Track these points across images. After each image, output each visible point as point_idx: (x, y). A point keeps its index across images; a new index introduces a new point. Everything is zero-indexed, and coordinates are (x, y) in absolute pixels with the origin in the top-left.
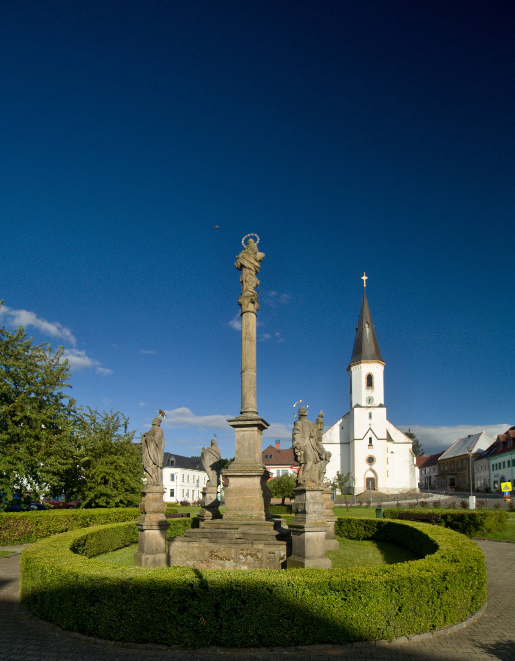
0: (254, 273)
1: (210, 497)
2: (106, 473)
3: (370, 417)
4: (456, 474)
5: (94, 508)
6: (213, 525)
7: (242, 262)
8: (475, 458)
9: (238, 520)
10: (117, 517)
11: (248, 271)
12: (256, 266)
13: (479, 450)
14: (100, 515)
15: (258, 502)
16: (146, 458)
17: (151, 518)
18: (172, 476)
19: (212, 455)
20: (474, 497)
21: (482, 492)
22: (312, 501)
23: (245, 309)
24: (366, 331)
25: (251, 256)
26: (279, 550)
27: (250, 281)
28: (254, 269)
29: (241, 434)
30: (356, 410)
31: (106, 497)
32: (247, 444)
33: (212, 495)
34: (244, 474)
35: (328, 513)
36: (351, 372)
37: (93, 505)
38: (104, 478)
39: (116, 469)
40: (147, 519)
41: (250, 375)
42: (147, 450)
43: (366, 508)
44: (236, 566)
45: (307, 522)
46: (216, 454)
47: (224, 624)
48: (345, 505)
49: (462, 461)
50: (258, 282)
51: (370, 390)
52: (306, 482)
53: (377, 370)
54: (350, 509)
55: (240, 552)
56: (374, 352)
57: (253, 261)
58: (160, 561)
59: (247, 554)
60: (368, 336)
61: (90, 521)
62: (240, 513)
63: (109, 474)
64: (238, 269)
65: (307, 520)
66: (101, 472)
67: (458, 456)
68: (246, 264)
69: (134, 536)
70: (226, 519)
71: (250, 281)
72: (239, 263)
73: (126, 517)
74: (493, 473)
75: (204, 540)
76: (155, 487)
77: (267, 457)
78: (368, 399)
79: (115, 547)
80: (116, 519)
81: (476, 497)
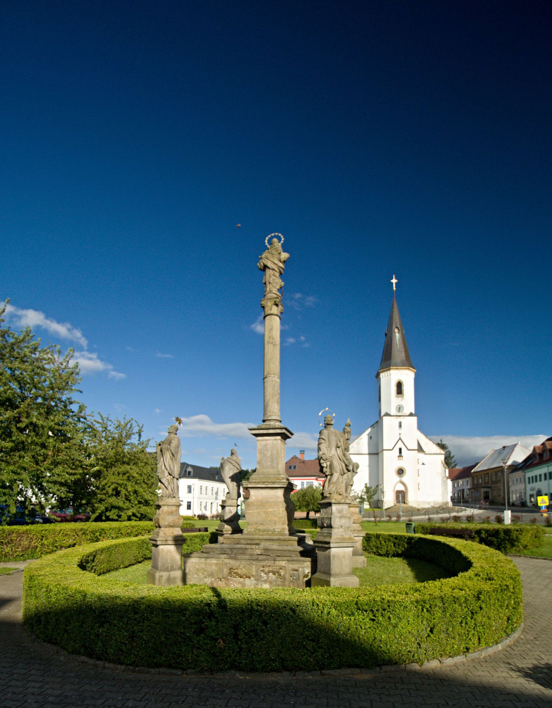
0: (277, 274)
1: (230, 510)
2: (118, 484)
4: (490, 487)
5: (105, 521)
6: (232, 540)
7: (265, 263)
10: (129, 531)
11: (271, 272)
12: (280, 267)
13: (514, 462)
16: (162, 468)
17: (166, 533)
18: (189, 488)
19: (232, 466)
20: (510, 511)
21: (517, 506)
24: (396, 336)
25: (275, 257)
26: (303, 567)
27: (274, 283)
28: (278, 270)
29: (263, 443)
30: (385, 419)
32: (269, 455)
33: (231, 508)
35: (355, 528)
36: (380, 379)
37: (104, 518)
38: (115, 489)
40: (161, 534)
41: (273, 381)
42: (162, 460)
44: (257, 584)
45: (333, 537)
46: (236, 465)
47: (244, 646)
48: (373, 519)
49: (496, 473)
50: (283, 284)
51: (400, 398)
52: (332, 495)
53: (407, 376)
55: (262, 569)
56: (404, 358)
57: (276, 262)
58: (175, 578)
59: (269, 572)
61: (100, 535)
62: (261, 527)
63: (121, 485)
64: (261, 269)
65: (333, 535)
66: (112, 483)
68: (269, 264)
70: (246, 534)
71: (274, 283)
72: (262, 264)
73: (139, 531)
76: (170, 499)
77: (290, 467)
78: (398, 407)
79: (127, 563)
80: (128, 534)
81: (512, 512)
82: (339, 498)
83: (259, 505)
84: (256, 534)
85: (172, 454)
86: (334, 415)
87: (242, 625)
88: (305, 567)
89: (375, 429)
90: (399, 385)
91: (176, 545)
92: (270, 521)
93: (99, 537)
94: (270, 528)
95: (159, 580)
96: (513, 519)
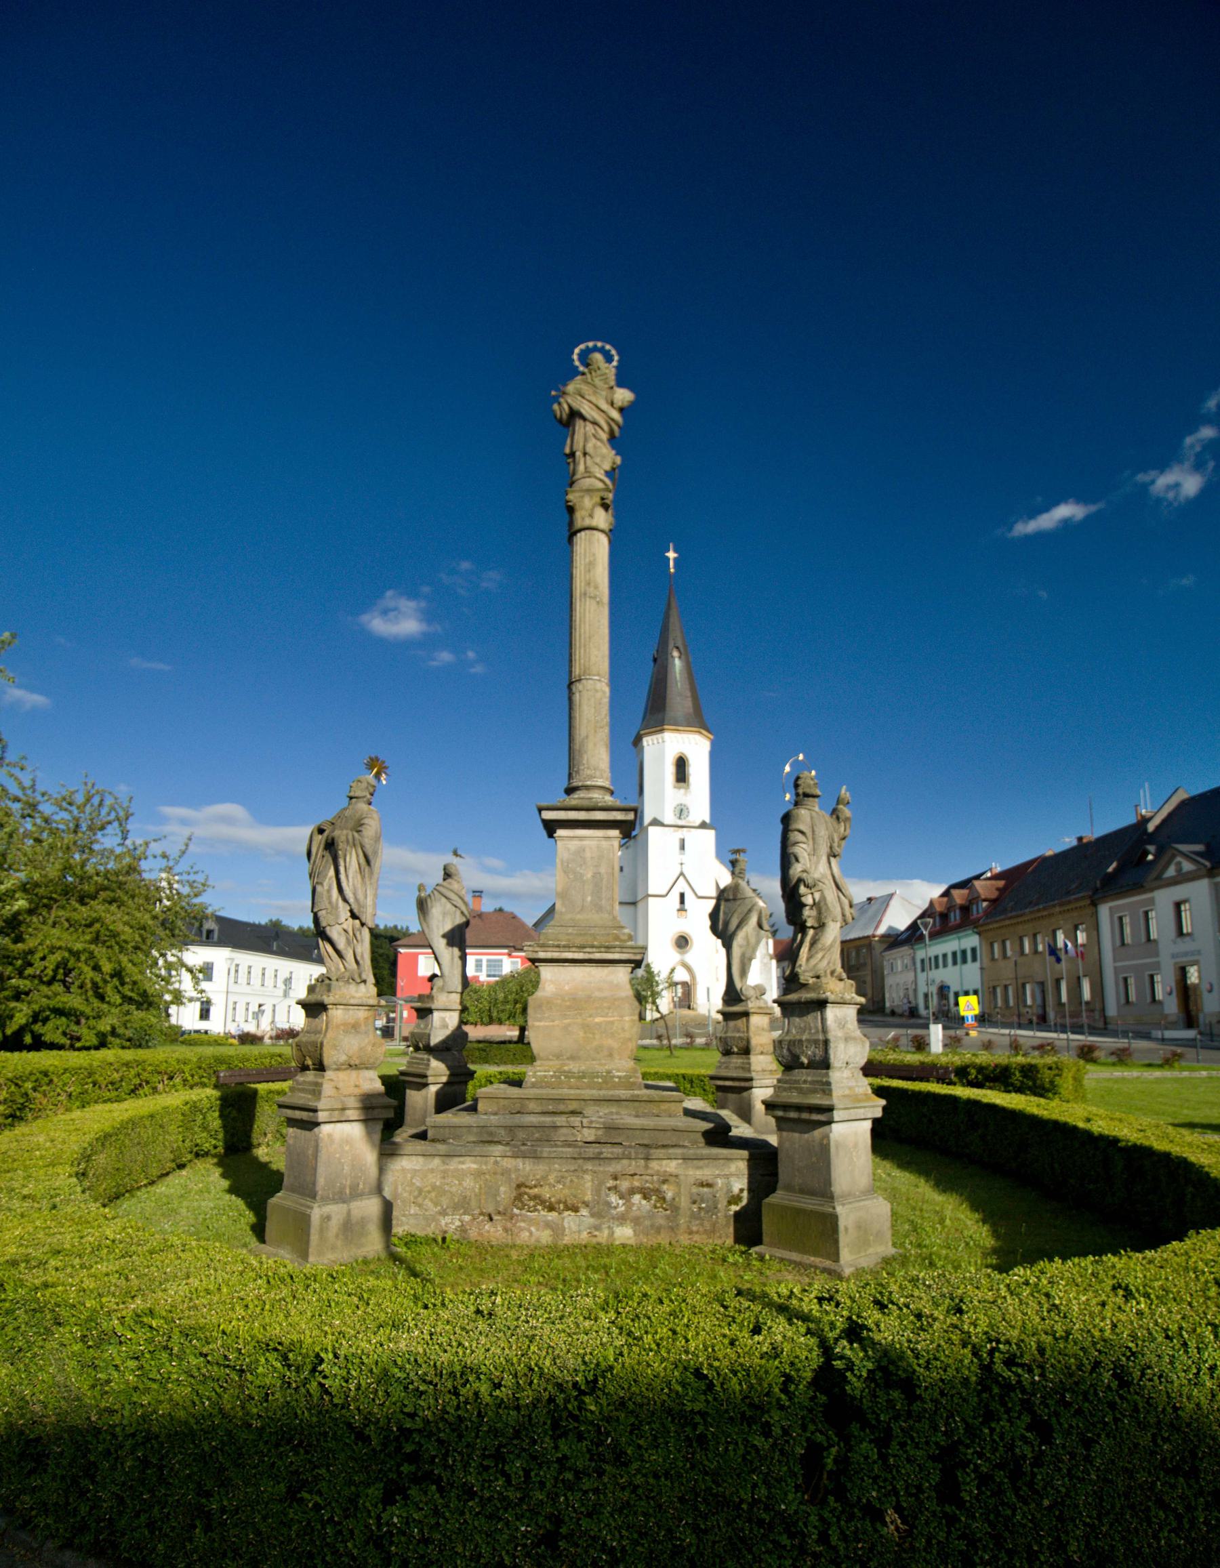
0: (604, 436)
1: (443, 1019)
2: (70, 951)
3: (682, 847)
5: (29, 1048)
6: (502, 1102)
7: (575, 405)
8: (885, 946)
9: (570, 1088)
10: (116, 1076)
11: (590, 428)
12: (613, 420)
13: (890, 928)
14: (66, 1070)
15: (627, 1035)
16: (330, 897)
17: (340, 1085)
19: (449, 906)
20: (940, 1026)
21: (901, 1015)
22: (840, 1034)
23: (581, 519)
25: (599, 396)
26: (727, 1176)
27: (596, 458)
28: (606, 427)
29: (573, 845)
30: (651, 829)
31: (64, 1019)
32: (589, 875)
33: (447, 1014)
34: (587, 956)
37: (28, 1039)
38: (63, 964)
39: (96, 939)
40: (327, 1089)
41: (596, 691)
42: (332, 872)
43: (703, 1049)
44: (597, 1228)
45: (835, 1094)
46: (460, 903)
47: (979, 1526)
48: (655, 1042)
49: (858, 949)
50: (618, 460)
51: (682, 791)
52: (823, 980)
54: (676, 1053)
55: (611, 1183)
56: (691, 710)
57: (605, 406)
58: (363, 1222)
59: (632, 1191)
60: (678, 676)
61: (35, 1089)
62: (573, 1066)
63: (76, 954)
64: (560, 421)
65: (833, 1087)
66: (53, 949)
67: (851, 940)
68: (586, 409)
69: (205, 1134)
70: (534, 1086)
71: (596, 458)
72: (566, 406)
73: (145, 1075)
74: (922, 977)
75: (498, 1149)
76: (352, 988)
79: (155, 1172)
80: (112, 1083)
81: (944, 1028)
82: (837, 989)
83: (569, 1007)
84: (559, 1085)
85: (366, 856)
86: (813, 773)
87: (968, 1447)
88: (732, 1175)
89: (630, 850)
90: (681, 765)
91: (365, 1121)
92: (598, 1049)
93: (32, 1094)
94: (598, 1068)
95: (322, 1231)
96: (948, 1042)
